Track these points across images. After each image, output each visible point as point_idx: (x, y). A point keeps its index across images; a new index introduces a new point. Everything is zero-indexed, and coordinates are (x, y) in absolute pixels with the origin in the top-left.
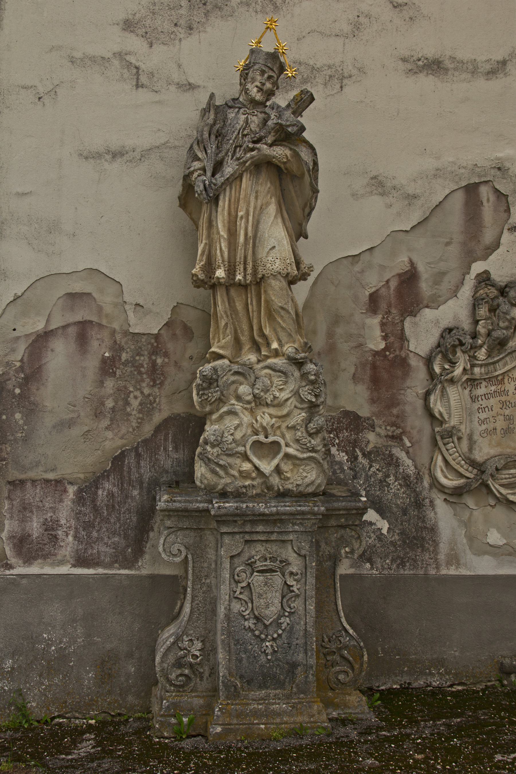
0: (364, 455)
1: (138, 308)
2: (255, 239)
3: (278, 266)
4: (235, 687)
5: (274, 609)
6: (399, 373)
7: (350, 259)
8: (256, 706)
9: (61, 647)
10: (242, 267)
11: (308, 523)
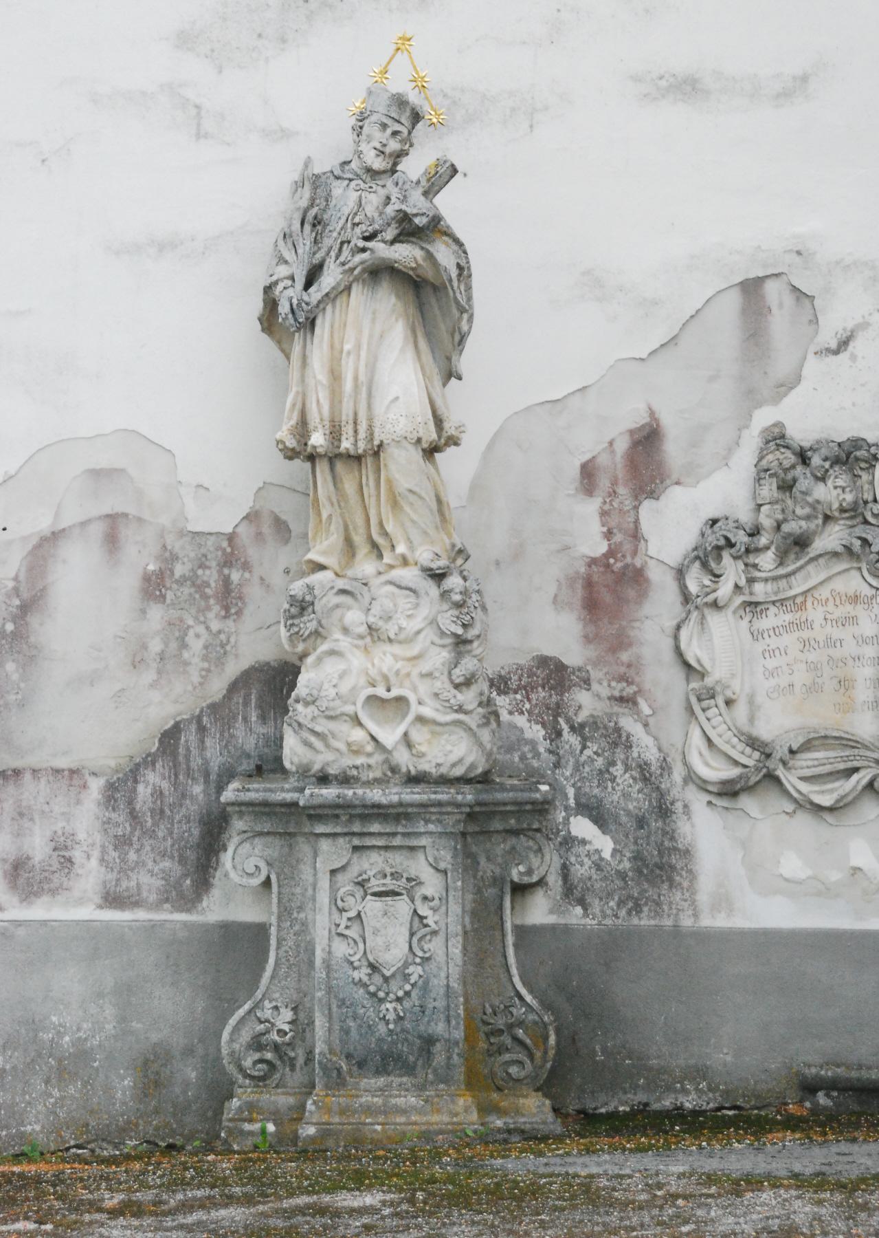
0: (572, 728)
1: (201, 491)
4: (339, 1070)
7: (549, 405)
8: (369, 1099)
9: (79, 1038)
10: (351, 432)
11: (450, 820)
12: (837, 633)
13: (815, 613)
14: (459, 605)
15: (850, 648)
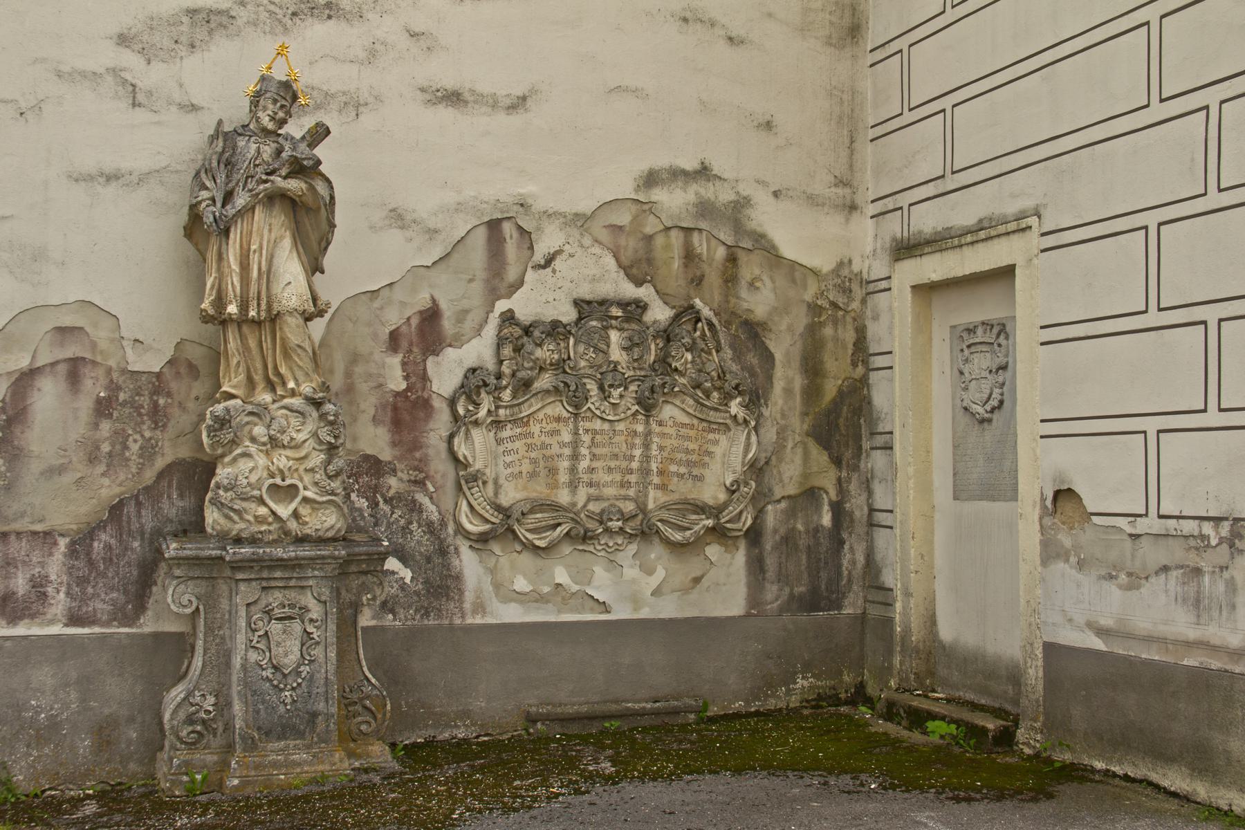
0: (385, 501)
1: (138, 344)
2: (268, 274)
3: (294, 302)
4: (253, 739)
5: (294, 657)
6: (422, 415)
11: (329, 568)
12: (548, 440)
13: (535, 429)
14: (332, 423)
15: (555, 449)
